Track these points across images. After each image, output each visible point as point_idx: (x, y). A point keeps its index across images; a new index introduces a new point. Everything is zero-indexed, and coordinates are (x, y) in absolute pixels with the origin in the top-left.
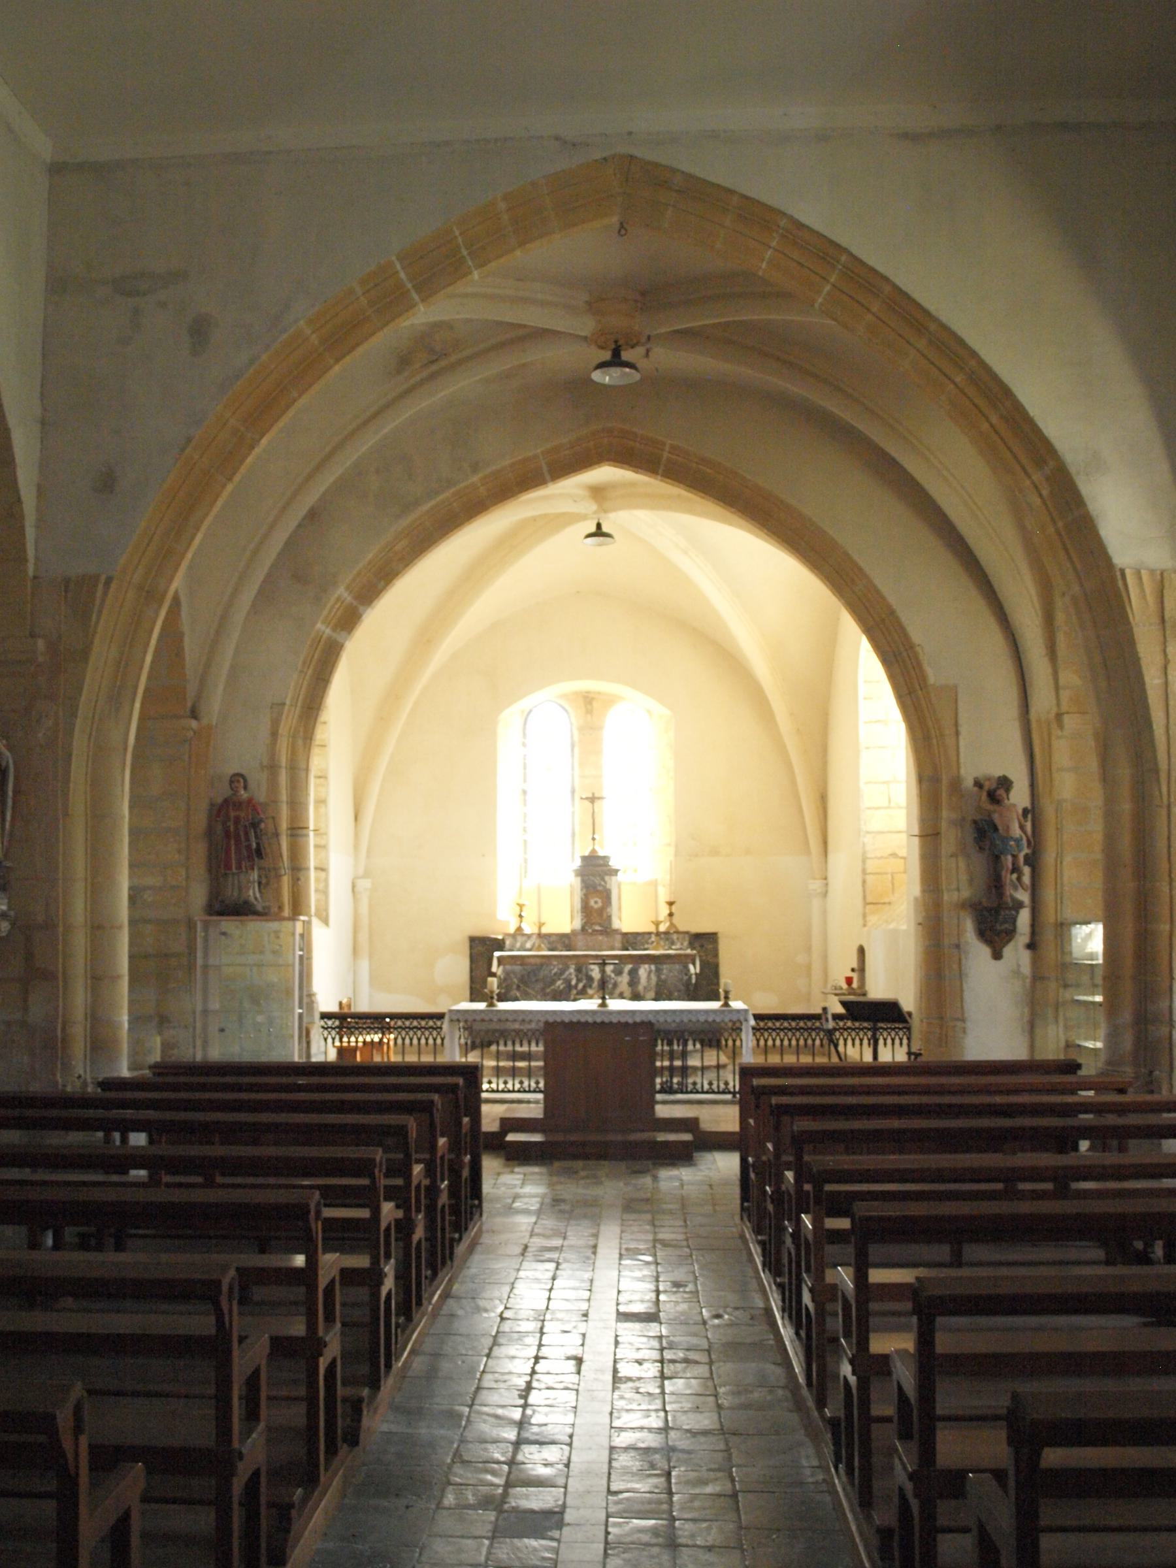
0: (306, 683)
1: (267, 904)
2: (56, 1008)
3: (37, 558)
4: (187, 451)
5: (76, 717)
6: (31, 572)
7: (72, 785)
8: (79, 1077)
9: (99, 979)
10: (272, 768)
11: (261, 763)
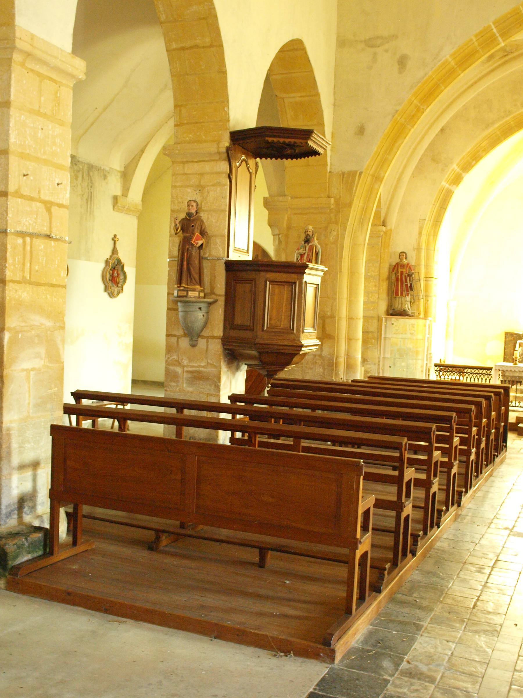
0: (435, 210)
1: (413, 311)
2: (334, 351)
3: (331, 164)
4: (395, 117)
5: (346, 231)
6: (329, 170)
7: (343, 259)
8: (341, 379)
9: (350, 340)
10: (418, 249)
11: (413, 247)
